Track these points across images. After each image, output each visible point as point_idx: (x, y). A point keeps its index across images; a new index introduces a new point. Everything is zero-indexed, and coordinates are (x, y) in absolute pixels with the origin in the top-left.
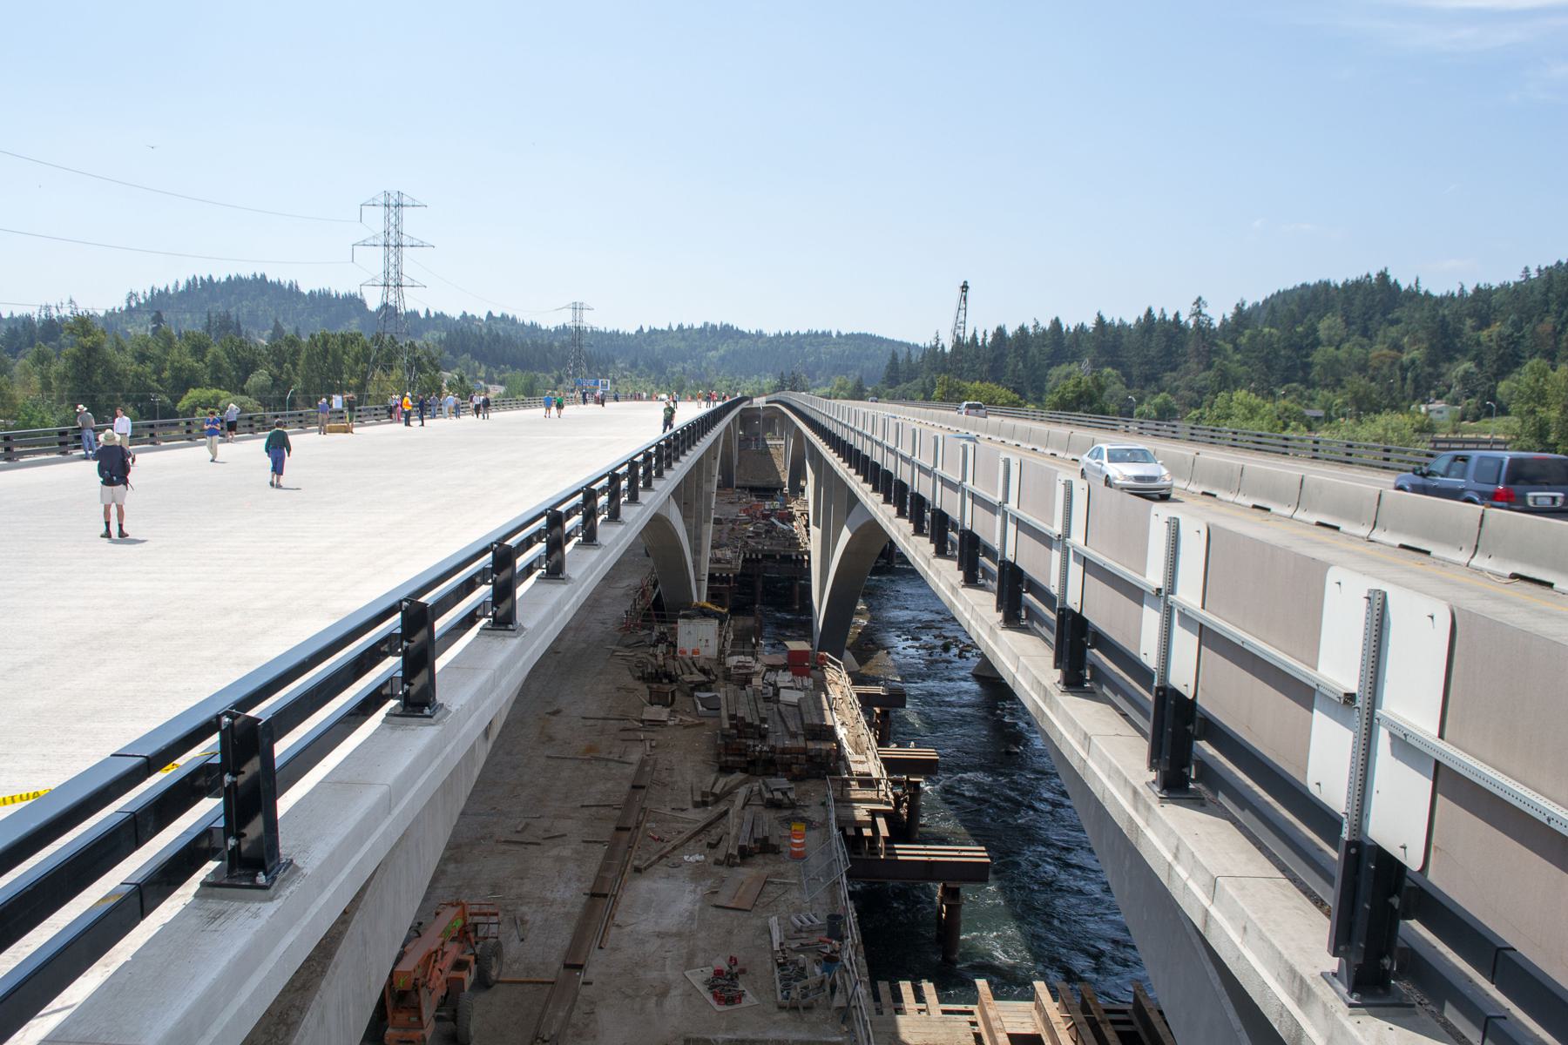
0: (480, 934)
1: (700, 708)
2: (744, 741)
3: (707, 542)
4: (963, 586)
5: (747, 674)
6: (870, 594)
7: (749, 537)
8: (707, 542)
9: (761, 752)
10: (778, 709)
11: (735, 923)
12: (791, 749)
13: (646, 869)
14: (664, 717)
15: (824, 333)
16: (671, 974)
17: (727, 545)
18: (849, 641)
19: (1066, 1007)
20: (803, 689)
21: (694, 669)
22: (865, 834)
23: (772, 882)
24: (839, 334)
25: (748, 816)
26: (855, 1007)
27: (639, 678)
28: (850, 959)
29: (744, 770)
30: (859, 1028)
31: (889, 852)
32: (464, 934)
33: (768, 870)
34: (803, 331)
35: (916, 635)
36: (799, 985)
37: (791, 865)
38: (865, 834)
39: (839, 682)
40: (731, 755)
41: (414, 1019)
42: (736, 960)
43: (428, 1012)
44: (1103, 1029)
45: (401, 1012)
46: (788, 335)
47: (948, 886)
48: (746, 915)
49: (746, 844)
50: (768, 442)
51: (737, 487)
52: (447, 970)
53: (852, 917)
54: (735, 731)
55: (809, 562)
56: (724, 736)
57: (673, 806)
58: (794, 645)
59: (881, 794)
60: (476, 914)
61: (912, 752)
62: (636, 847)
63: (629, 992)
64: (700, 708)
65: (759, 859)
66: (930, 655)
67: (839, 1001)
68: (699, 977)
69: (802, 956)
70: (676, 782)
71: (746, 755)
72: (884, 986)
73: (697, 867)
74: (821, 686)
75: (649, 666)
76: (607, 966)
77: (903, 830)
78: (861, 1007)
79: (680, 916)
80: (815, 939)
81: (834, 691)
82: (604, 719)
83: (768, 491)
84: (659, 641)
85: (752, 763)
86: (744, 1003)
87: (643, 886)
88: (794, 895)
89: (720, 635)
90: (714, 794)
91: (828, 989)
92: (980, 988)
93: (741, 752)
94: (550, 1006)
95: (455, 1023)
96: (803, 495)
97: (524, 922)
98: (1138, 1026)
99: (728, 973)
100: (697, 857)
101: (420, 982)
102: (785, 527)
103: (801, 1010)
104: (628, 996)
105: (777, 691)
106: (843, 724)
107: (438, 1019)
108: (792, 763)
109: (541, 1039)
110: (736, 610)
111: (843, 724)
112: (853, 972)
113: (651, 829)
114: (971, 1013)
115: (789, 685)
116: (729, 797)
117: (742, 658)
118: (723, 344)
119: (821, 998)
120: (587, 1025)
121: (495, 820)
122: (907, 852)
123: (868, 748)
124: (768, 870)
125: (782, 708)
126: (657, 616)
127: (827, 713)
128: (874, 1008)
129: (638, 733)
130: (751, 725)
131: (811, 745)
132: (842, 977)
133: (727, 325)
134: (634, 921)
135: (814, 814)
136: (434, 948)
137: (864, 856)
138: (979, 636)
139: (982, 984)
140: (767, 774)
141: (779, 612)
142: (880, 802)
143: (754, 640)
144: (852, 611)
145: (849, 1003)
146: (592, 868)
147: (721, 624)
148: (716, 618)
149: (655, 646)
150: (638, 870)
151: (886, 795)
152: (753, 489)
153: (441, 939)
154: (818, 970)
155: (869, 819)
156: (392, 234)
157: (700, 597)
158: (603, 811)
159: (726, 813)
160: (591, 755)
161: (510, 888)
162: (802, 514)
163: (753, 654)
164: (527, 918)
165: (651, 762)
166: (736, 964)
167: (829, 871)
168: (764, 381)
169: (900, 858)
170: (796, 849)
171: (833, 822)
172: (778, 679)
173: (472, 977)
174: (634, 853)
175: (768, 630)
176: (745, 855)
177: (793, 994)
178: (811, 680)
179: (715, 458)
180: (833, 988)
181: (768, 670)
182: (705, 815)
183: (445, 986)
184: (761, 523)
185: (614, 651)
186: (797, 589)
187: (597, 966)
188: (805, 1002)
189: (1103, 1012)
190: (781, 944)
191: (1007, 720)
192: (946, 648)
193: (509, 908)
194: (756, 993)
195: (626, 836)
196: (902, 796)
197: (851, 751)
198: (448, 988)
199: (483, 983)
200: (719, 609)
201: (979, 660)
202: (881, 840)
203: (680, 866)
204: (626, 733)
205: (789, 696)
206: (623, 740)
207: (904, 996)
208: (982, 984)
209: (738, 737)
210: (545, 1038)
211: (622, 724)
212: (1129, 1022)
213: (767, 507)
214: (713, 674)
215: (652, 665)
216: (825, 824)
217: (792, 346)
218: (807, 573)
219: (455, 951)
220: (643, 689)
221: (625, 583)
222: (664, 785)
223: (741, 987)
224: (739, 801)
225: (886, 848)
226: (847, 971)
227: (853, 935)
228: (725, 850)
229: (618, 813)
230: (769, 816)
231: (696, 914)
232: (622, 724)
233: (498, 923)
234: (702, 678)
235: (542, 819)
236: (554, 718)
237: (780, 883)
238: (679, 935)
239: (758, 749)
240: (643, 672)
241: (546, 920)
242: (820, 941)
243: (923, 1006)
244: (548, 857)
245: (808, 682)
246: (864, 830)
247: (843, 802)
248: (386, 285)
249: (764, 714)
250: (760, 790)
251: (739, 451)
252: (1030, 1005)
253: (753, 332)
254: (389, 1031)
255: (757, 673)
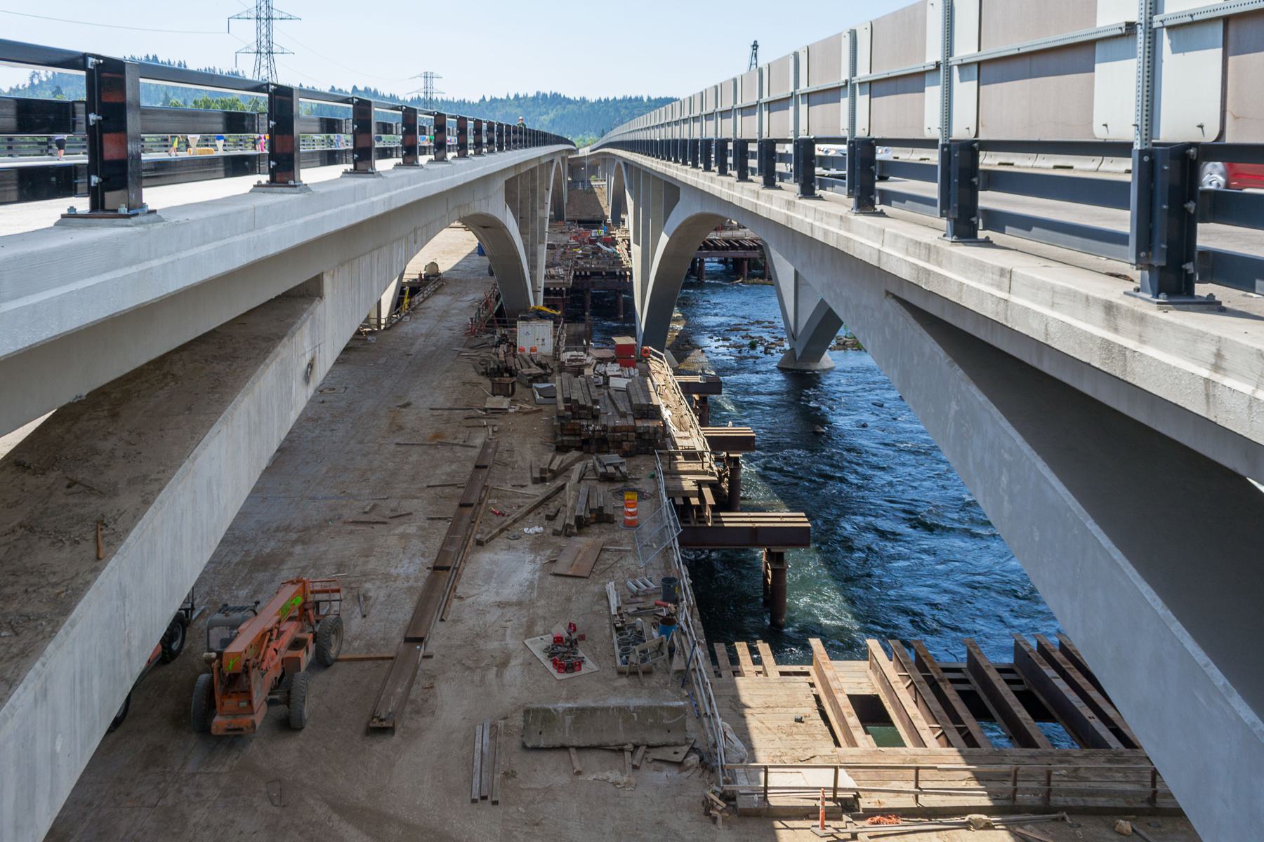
0: (322, 612)
1: (538, 397)
2: (578, 421)
3: (542, 259)
4: (800, 198)
5: (580, 366)
6: (684, 304)
7: (578, 258)
8: (542, 259)
9: (594, 431)
10: (609, 393)
11: (573, 590)
12: (621, 427)
13: (487, 542)
14: (505, 406)
15: (636, 98)
16: (512, 643)
17: (559, 265)
18: (667, 346)
19: (902, 666)
20: (631, 377)
21: (532, 364)
22: (693, 503)
23: (608, 550)
24: (649, 98)
25: (583, 488)
26: (694, 670)
27: (482, 374)
28: (686, 621)
29: (579, 449)
30: (699, 692)
31: (716, 519)
32: (306, 612)
33: (602, 539)
34: (619, 97)
35: (725, 337)
36: (637, 648)
37: (625, 533)
38: (693, 503)
39: (662, 372)
40: (566, 435)
41: (244, 704)
42: (574, 626)
43: (259, 694)
44: (943, 688)
45: (230, 697)
46: (607, 101)
47: (772, 550)
48: (583, 582)
49: (583, 514)
50: (593, 183)
51: (567, 221)
52: (283, 649)
53: (686, 581)
54: (570, 413)
55: (631, 277)
56: (560, 418)
57: (514, 482)
58: (620, 340)
59: (706, 465)
60: (318, 592)
61: (730, 430)
62: (478, 522)
63: (470, 663)
64: (538, 397)
65: (595, 529)
66: (739, 352)
67: (678, 663)
68: (538, 646)
69: (639, 619)
70: (517, 461)
71: (580, 435)
72: (720, 648)
73: (536, 538)
74: (646, 373)
75: (492, 363)
76: (449, 638)
77: (727, 502)
78: (700, 670)
79: (521, 585)
80: (651, 603)
81: (658, 379)
82: (449, 409)
83: (596, 223)
84: (500, 342)
85: (586, 442)
86: (584, 670)
87: (484, 559)
88: (629, 562)
89: (555, 337)
90: (551, 471)
91: (666, 652)
92: (814, 648)
93: (575, 432)
94: (389, 681)
95: (288, 707)
96: (624, 224)
97: (366, 598)
98: (975, 685)
99: (567, 640)
100: (537, 529)
101: (251, 663)
102: (609, 250)
103: (641, 674)
104: (469, 668)
105: (607, 379)
106: (667, 407)
107: (271, 703)
108: (623, 441)
109: (378, 717)
110: (572, 318)
111: (667, 407)
112: (690, 634)
113: (493, 504)
114: (807, 674)
115: (618, 373)
116: (566, 474)
117: (575, 353)
118: (552, 110)
119: (660, 661)
120: (426, 701)
121: (344, 502)
122: (732, 520)
123: (691, 427)
124: (602, 539)
125: (612, 393)
126: (499, 322)
127: (653, 395)
128: (712, 670)
129: (482, 420)
130: (583, 407)
131: (639, 423)
132: (680, 641)
133: (556, 94)
134: (476, 592)
135: (645, 485)
136: (269, 626)
137: (693, 524)
138: (826, 232)
139: (816, 643)
140: (600, 451)
141: (607, 321)
142: (705, 473)
143: (585, 342)
144: (668, 319)
145: (688, 666)
146: (436, 543)
147: (556, 327)
148: (550, 319)
149: (497, 346)
150: (480, 543)
151: (710, 467)
152: (580, 222)
153: (277, 618)
154: (655, 633)
155: (696, 488)
156: (264, 9)
157: (536, 301)
158: (447, 490)
159: (563, 487)
160: (438, 440)
161: (355, 566)
162: (624, 240)
163: (585, 350)
164: (370, 594)
165: (493, 445)
166: (575, 630)
167: (661, 538)
168: (587, 139)
169: (726, 525)
170: (629, 518)
171: (663, 491)
172: (607, 369)
173: (310, 656)
174: (476, 527)
175: (597, 336)
176: (582, 525)
177: (632, 658)
178: (637, 370)
179: (548, 190)
180: (672, 650)
181: (598, 363)
182: (542, 491)
183: (280, 667)
184: (589, 247)
185: (461, 352)
186: (622, 301)
187: (438, 637)
188: (644, 666)
189: (940, 671)
190: (619, 608)
191: (812, 404)
192: (753, 346)
193: (353, 585)
194: (596, 659)
195: (469, 511)
196: (723, 472)
197: (675, 429)
198: (283, 669)
199: (322, 662)
200: (554, 312)
201: (782, 355)
202: (708, 509)
203: (520, 537)
204: (470, 420)
205: (620, 383)
206: (468, 427)
207: (740, 657)
208: (816, 643)
209: (573, 419)
210: (383, 716)
211: (467, 413)
212: (966, 681)
213: (593, 235)
214: (546, 368)
215: (494, 362)
216: (655, 495)
217: (610, 110)
218: (629, 290)
219: (293, 630)
220: (487, 382)
221: (471, 297)
222: (506, 465)
223: (581, 654)
224: (575, 476)
225: (712, 517)
226: (684, 634)
227: (688, 598)
228: (562, 521)
229: (462, 491)
230: (603, 489)
231: (536, 583)
232: (467, 413)
233: (340, 600)
234: (540, 371)
235: (388, 501)
236: (404, 410)
237: (616, 550)
238: (519, 604)
239: (591, 428)
240: (486, 369)
241: (389, 596)
242: (656, 605)
243: (760, 668)
244: (394, 535)
245: (635, 372)
246: (691, 499)
247: (671, 474)
248: (259, 52)
249: (595, 396)
250: (594, 466)
251: (569, 190)
252: (865, 664)
253: (578, 99)
254: (217, 719)
255: (588, 365)
